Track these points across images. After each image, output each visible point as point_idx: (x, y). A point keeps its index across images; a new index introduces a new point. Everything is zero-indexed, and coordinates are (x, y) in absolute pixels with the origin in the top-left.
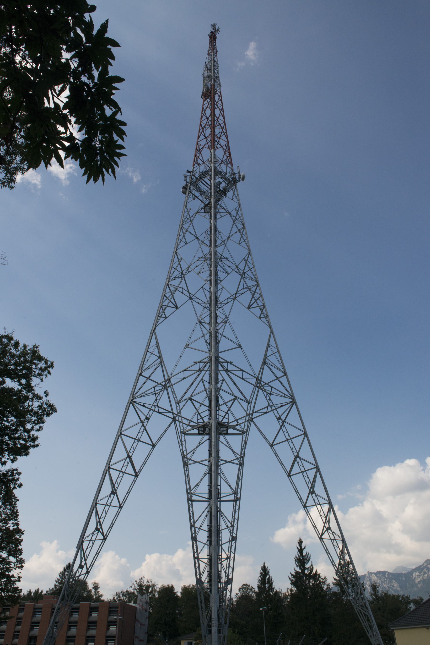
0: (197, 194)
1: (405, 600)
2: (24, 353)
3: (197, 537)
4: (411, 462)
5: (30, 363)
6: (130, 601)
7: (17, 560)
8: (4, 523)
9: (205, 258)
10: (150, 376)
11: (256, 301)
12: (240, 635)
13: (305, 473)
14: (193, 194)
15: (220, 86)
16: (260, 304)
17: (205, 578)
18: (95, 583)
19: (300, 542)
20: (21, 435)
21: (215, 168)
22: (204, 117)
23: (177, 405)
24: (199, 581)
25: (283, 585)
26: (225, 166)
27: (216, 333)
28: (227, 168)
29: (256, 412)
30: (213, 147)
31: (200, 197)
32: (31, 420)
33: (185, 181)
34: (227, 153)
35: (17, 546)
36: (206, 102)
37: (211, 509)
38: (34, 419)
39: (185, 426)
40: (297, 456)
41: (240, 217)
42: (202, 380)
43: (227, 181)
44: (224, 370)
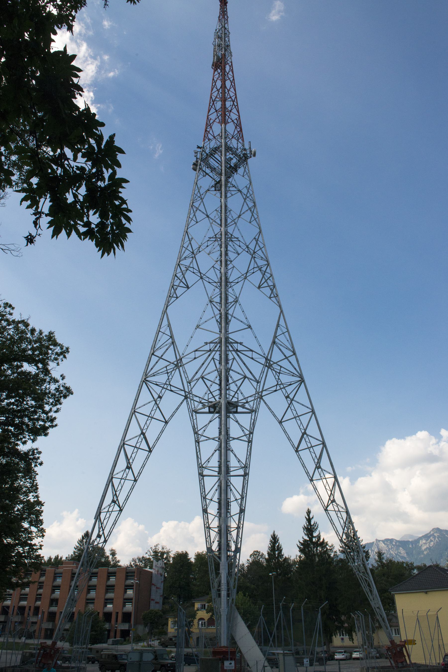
0: (208, 171)
1: (409, 566)
2: (39, 340)
3: (208, 509)
4: (422, 434)
5: (46, 348)
6: (146, 566)
7: (38, 529)
8: (25, 496)
9: (216, 238)
10: (162, 356)
11: (266, 281)
12: (250, 598)
13: (311, 448)
14: (203, 171)
15: (231, 55)
16: (270, 283)
17: (215, 547)
18: (112, 550)
19: (309, 512)
20: (40, 416)
21: (226, 144)
22: (215, 89)
23: (189, 385)
24: (209, 549)
25: (291, 552)
26: (236, 141)
27: (226, 314)
28: (238, 144)
29: (265, 390)
30: (224, 121)
31: (211, 174)
32: (49, 402)
33: (195, 158)
34: (238, 127)
35: (37, 517)
36: (216, 73)
37: (221, 483)
38: (51, 401)
39: (196, 404)
40: (304, 433)
41: (251, 195)
42: (213, 358)
43: (237, 157)
44: (234, 350)
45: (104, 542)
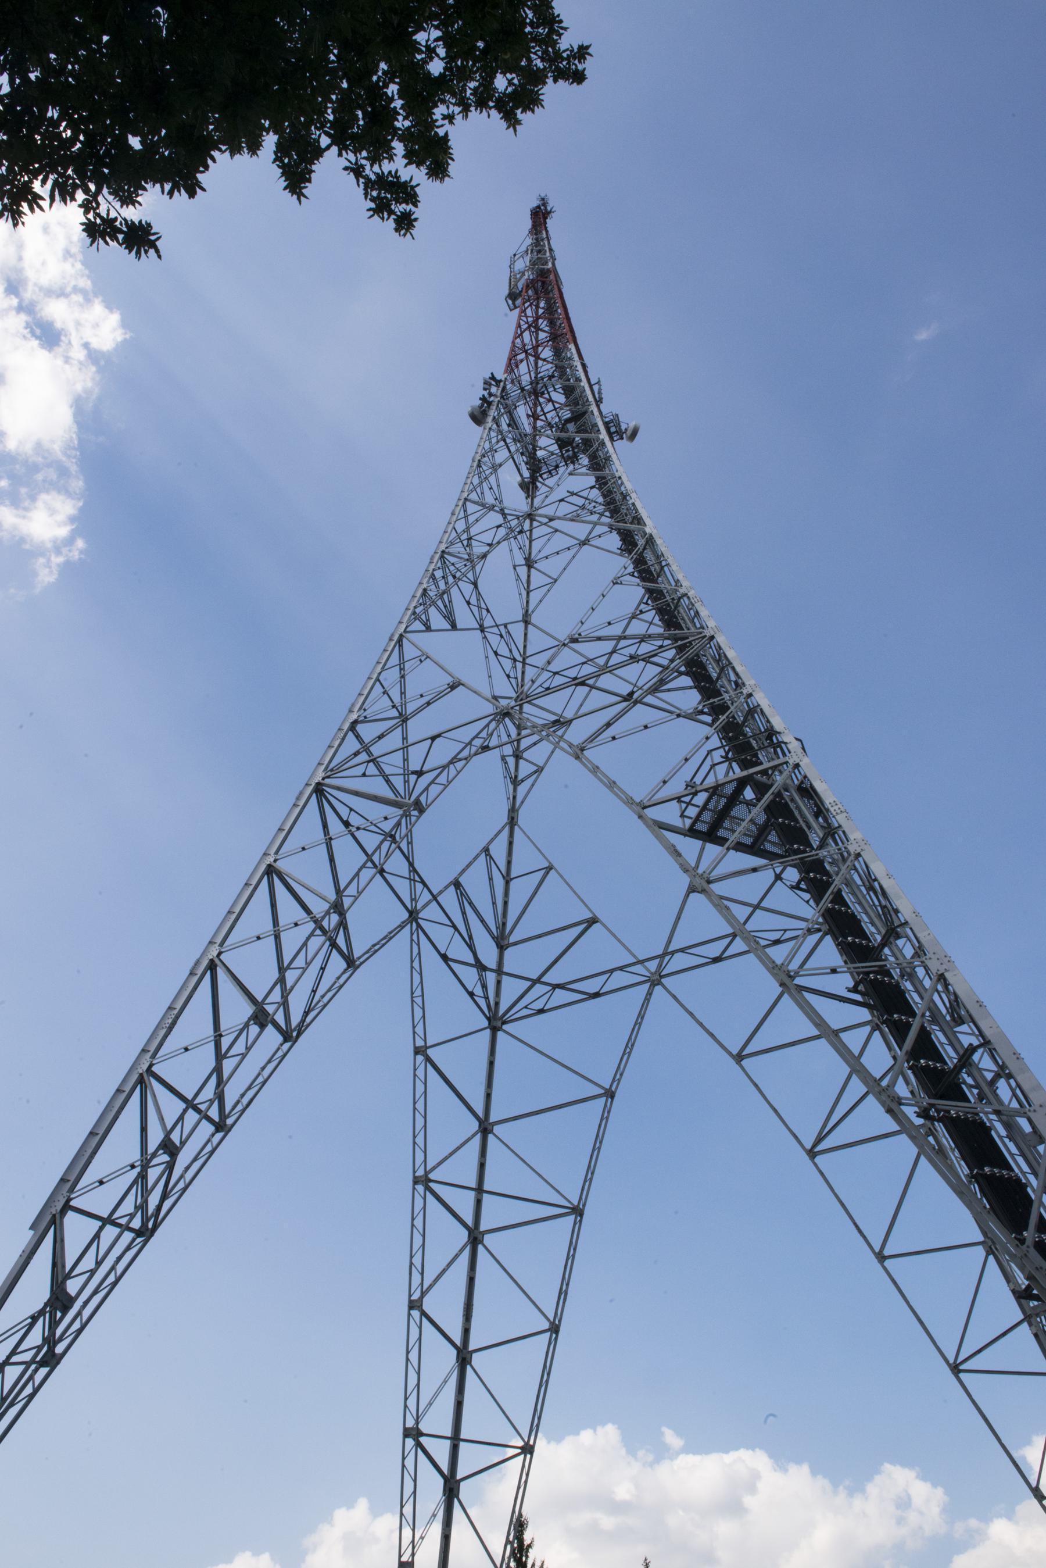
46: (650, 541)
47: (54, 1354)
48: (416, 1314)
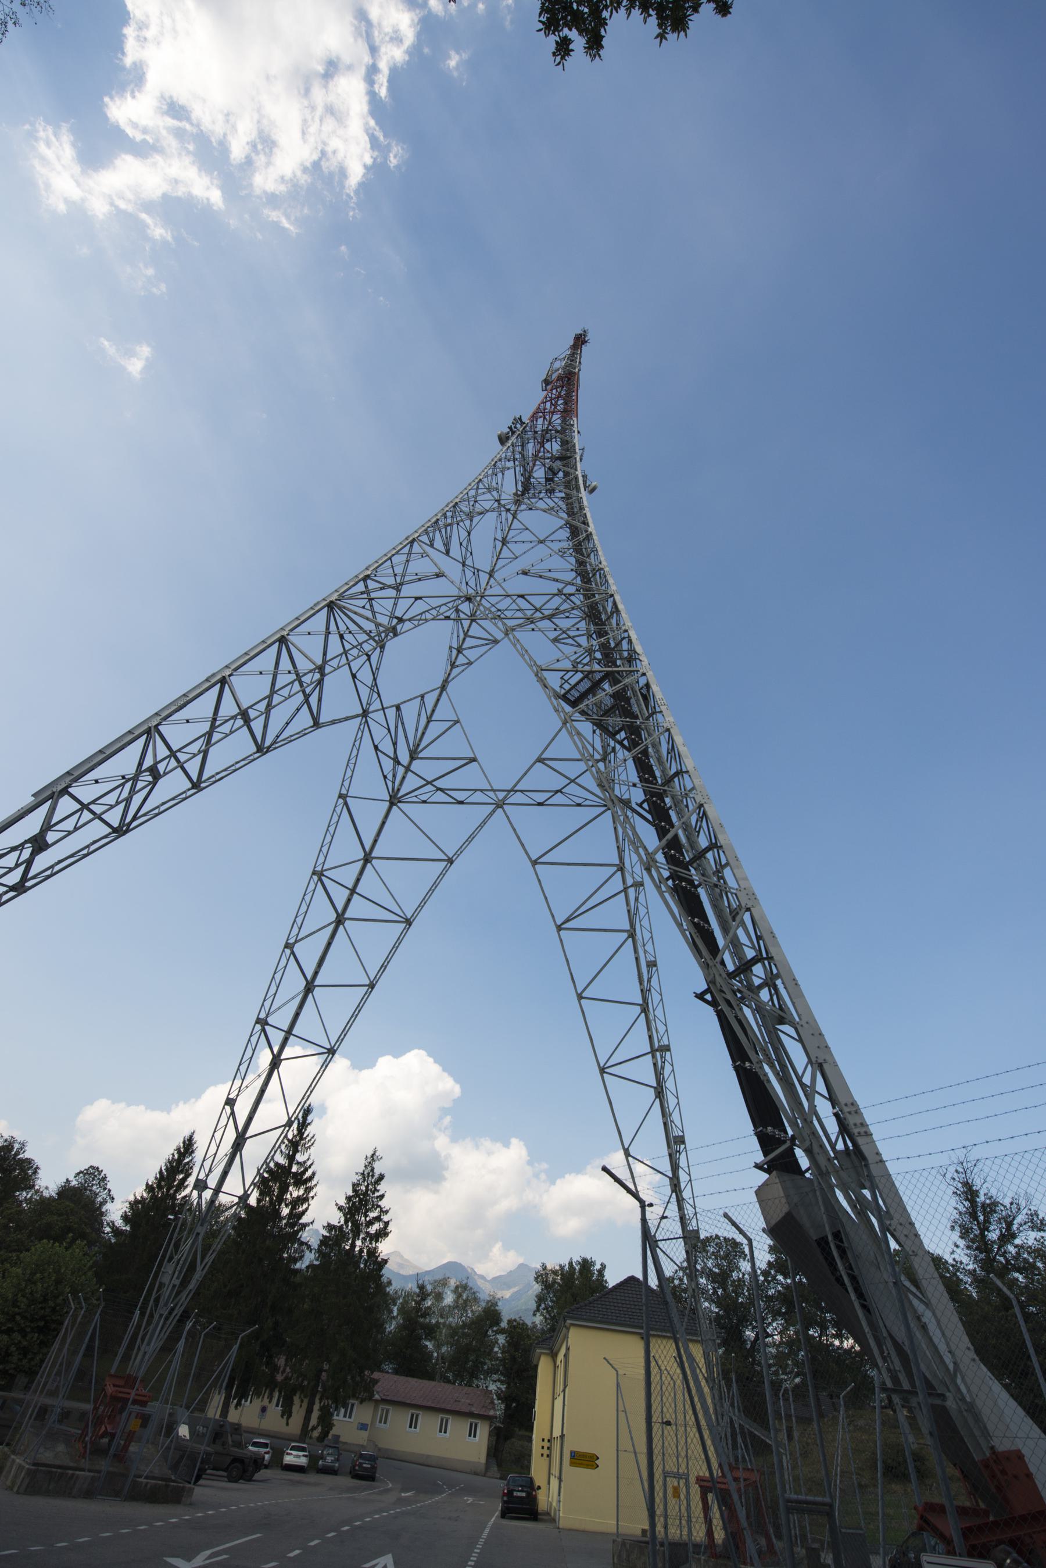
45: (12, 888)
46: (589, 537)
47: (24, 886)
48: (288, 951)
